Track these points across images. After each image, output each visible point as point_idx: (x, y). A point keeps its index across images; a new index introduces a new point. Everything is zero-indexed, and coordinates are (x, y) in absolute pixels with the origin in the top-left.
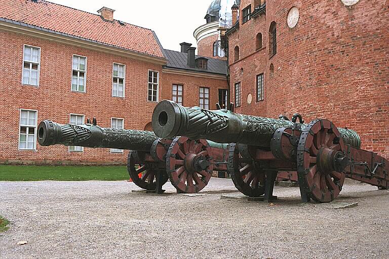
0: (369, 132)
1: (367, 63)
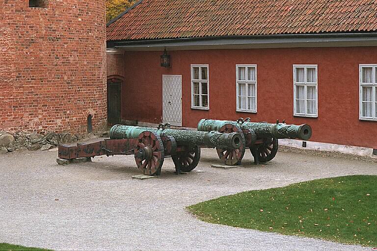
0: (10, 99)
1: (9, 24)
